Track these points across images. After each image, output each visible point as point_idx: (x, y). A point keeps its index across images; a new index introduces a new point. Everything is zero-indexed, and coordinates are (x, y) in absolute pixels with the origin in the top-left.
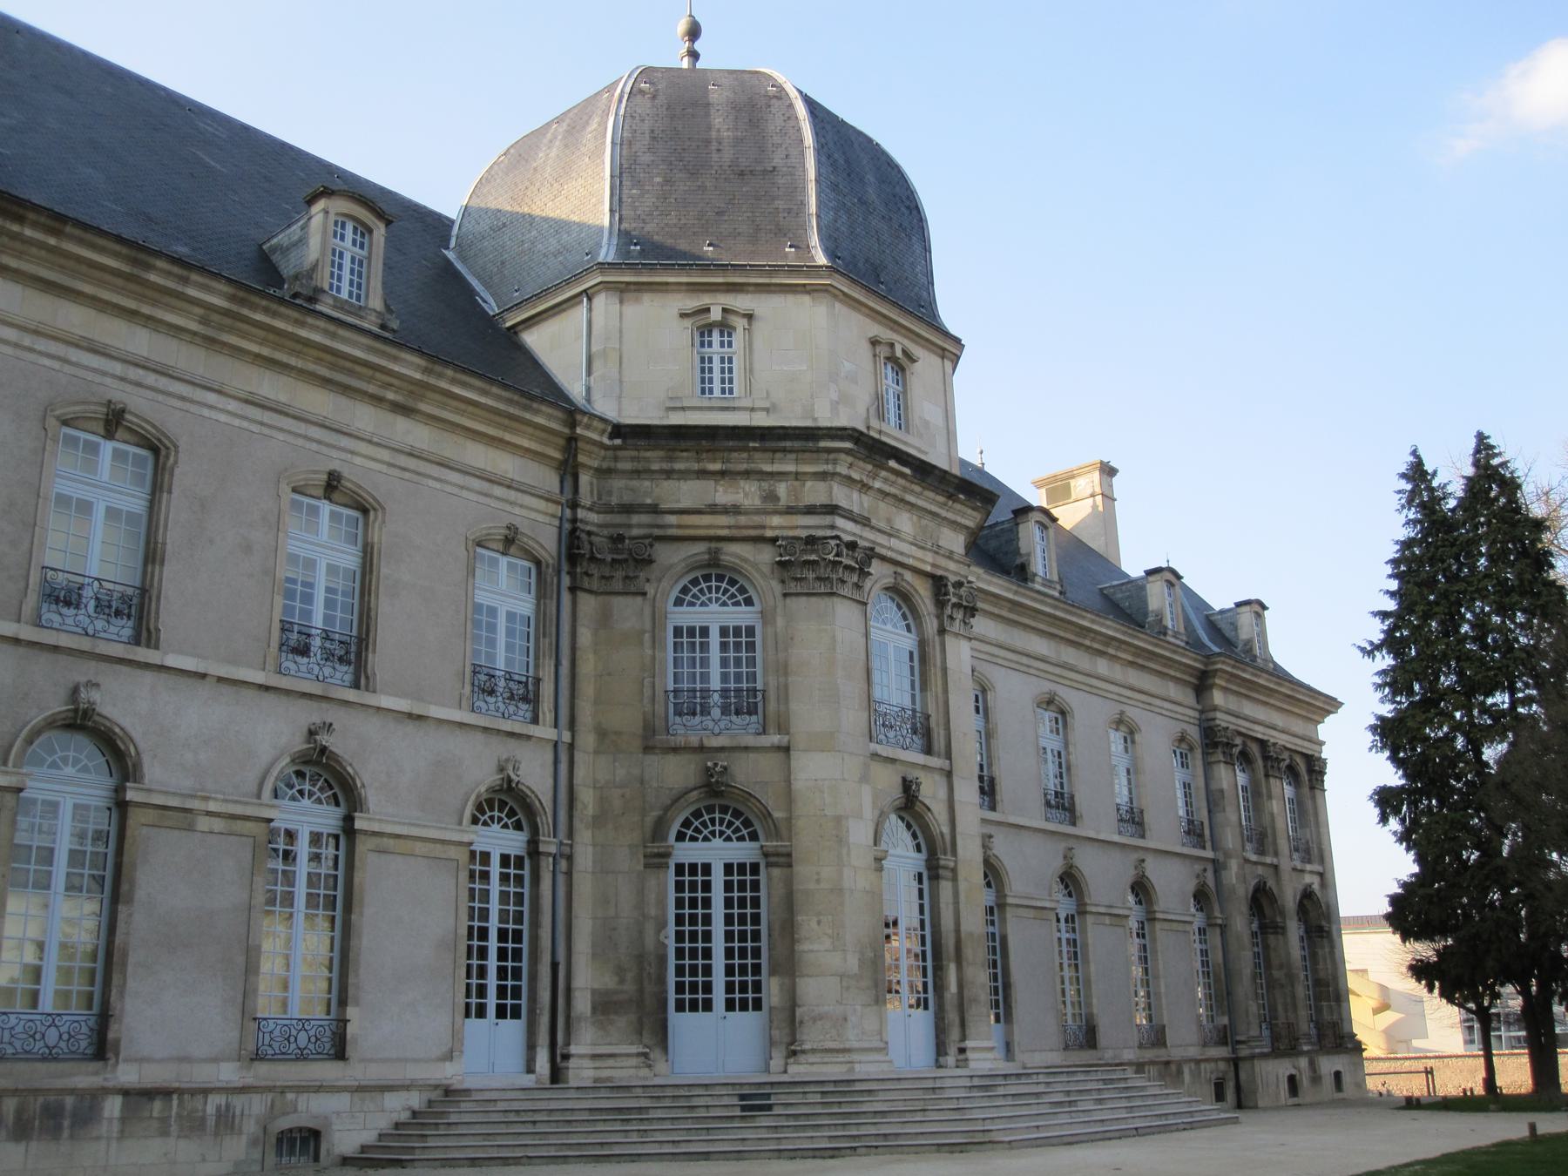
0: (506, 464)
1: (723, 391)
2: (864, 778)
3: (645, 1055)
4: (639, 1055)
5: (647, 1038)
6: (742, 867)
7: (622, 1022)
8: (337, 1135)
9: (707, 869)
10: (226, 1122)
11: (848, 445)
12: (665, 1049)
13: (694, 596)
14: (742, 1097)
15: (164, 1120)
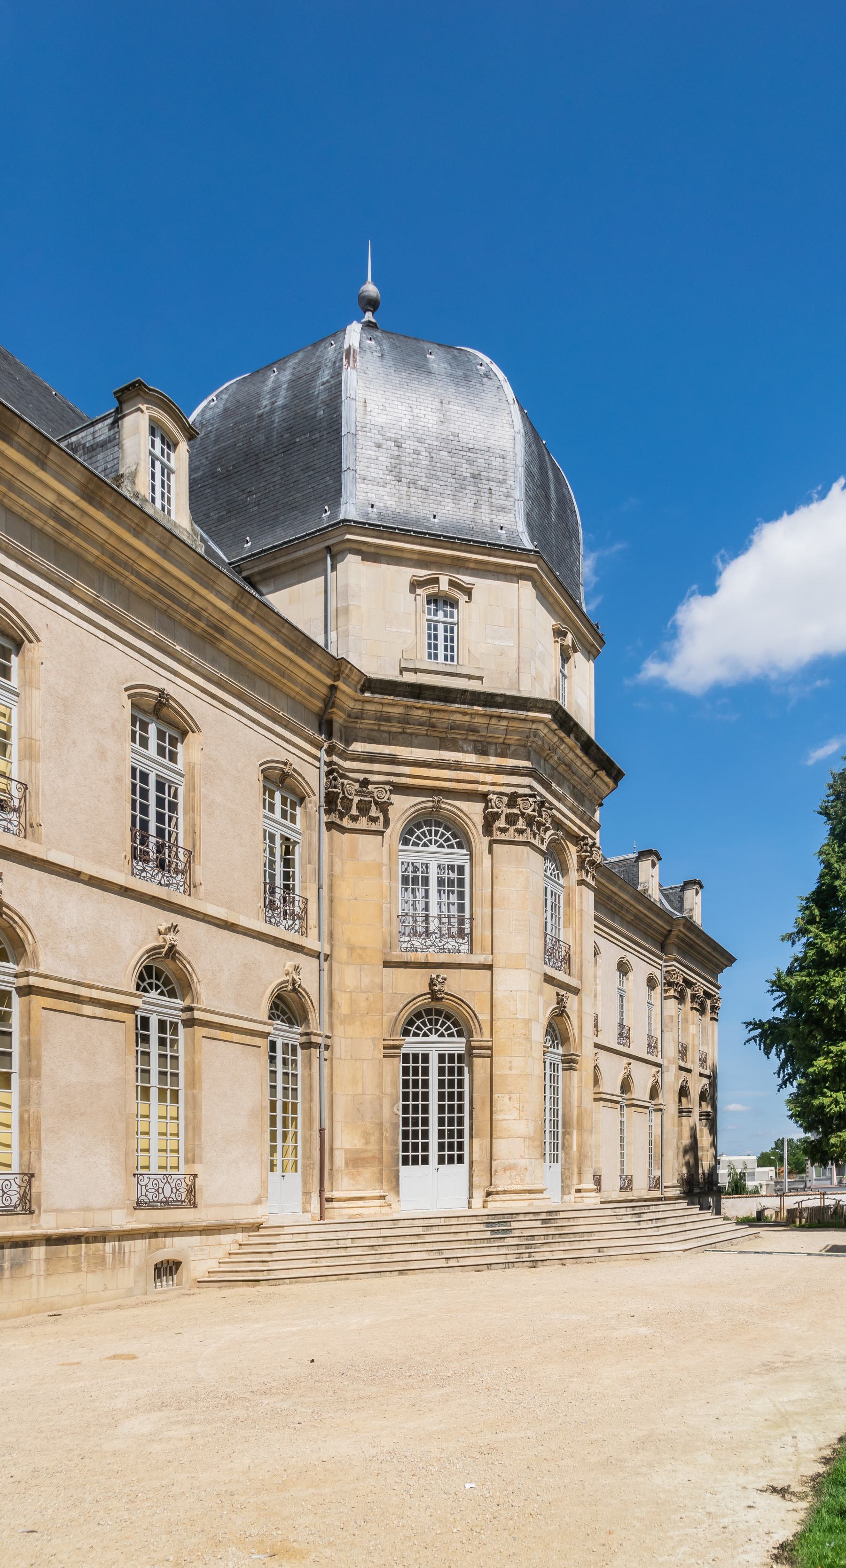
1: (446, 659)
3: (384, 1197)
5: (385, 1186)
8: (193, 1264)
9: (426, 1058)
12: (398, 1193)
13: (418, 838)
15: (77, 1259)
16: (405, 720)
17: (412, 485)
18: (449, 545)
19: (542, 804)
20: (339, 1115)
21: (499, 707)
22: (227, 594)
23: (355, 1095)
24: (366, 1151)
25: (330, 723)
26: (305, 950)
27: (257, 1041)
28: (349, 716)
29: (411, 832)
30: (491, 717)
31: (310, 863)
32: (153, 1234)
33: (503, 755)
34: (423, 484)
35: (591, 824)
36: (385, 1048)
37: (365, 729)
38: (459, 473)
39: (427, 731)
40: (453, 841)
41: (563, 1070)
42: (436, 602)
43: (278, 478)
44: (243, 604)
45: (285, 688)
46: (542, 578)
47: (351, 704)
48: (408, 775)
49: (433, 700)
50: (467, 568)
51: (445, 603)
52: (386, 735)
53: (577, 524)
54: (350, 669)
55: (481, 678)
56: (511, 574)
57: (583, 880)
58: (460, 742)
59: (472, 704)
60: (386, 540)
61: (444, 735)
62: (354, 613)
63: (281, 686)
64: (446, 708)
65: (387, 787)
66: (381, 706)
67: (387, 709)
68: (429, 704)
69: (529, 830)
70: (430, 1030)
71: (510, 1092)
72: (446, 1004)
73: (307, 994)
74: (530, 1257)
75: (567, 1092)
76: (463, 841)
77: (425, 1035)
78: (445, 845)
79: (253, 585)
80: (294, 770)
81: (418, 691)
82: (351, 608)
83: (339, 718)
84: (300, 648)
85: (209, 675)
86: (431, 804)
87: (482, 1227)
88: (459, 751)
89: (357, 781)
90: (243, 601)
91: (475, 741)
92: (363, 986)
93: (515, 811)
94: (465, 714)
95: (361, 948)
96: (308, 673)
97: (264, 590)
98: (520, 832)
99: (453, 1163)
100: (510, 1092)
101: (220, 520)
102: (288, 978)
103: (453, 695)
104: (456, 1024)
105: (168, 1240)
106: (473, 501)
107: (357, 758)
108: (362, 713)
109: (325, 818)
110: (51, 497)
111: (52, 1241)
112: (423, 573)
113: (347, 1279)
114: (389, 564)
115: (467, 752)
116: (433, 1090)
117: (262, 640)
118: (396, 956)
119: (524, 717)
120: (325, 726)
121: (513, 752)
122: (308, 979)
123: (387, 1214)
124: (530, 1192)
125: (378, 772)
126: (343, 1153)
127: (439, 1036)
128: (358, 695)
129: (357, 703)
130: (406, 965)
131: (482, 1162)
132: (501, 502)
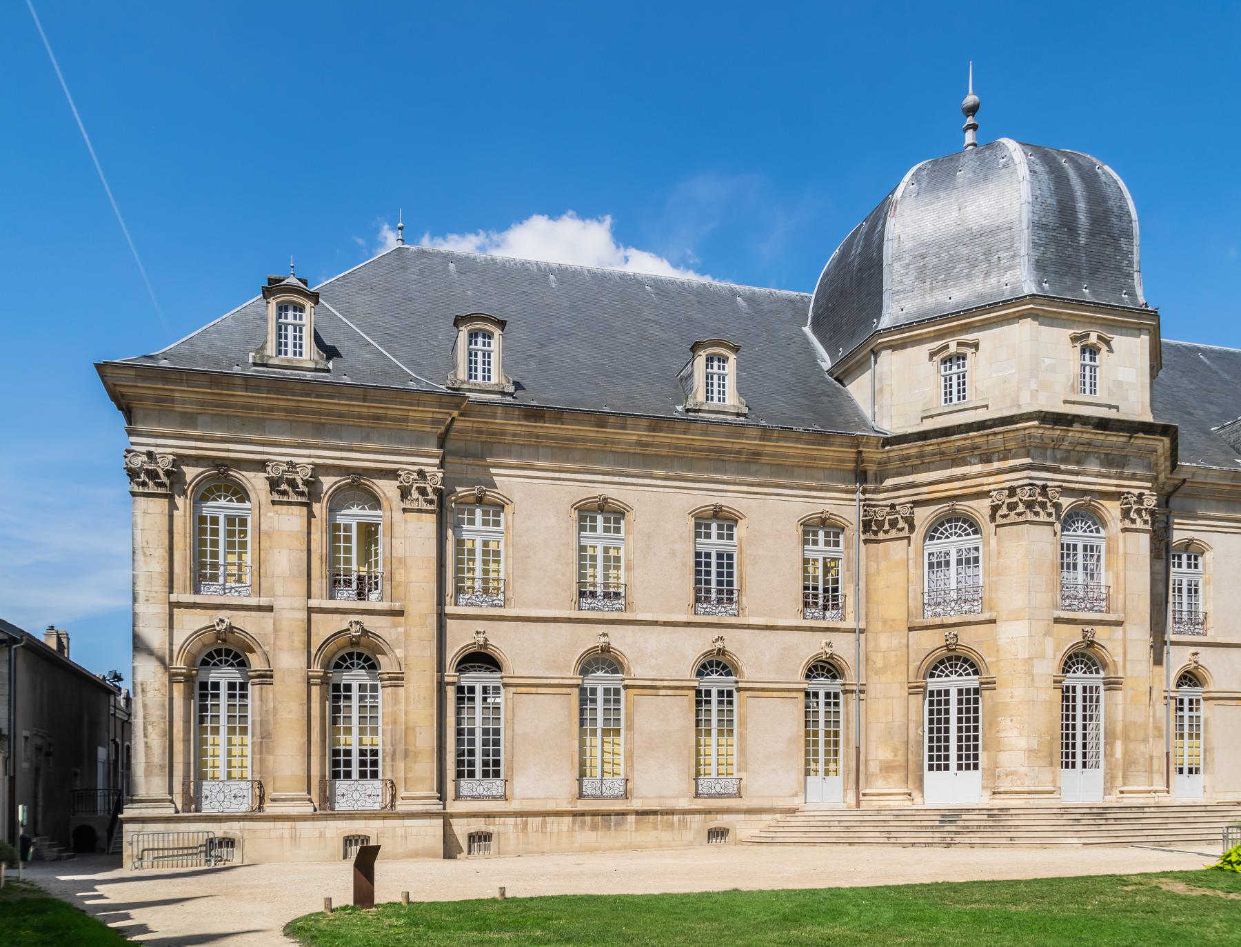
5: (911, 785)
6: (968, 691)
7: (897, 776)
9: (947, 693)
10: (683, 825)
11: (1036, 423)
12: (922, 791)
13: (942, 533)
14: (943, 815)
15: (655, 823)
16: (921, 455)
20: (873, 736)
25: (865, 472)
27: (794, 694)
29: (936, 530)
32: (708, 812)
33: (1005, 459)
48: (925, 493)
51: (958, 359)
55: (987, 406)
68: (934, 441)
72: (960, 652)
76: (974, 527)
77: (947, 676)
79: (840, 382)
81: (924, 436)
83: (872, 468)
87: (939, 818)
93: (1015, 499)
104: (972, 665)
105: (719, 816)
107: (887, 490)
109: (863, 537)
110: (634, 438)
111: (638, 813)
120: (861, 476)
122: (843, 648)
124: (1029, 793)
125: (904, 497)
130: (927, 628)
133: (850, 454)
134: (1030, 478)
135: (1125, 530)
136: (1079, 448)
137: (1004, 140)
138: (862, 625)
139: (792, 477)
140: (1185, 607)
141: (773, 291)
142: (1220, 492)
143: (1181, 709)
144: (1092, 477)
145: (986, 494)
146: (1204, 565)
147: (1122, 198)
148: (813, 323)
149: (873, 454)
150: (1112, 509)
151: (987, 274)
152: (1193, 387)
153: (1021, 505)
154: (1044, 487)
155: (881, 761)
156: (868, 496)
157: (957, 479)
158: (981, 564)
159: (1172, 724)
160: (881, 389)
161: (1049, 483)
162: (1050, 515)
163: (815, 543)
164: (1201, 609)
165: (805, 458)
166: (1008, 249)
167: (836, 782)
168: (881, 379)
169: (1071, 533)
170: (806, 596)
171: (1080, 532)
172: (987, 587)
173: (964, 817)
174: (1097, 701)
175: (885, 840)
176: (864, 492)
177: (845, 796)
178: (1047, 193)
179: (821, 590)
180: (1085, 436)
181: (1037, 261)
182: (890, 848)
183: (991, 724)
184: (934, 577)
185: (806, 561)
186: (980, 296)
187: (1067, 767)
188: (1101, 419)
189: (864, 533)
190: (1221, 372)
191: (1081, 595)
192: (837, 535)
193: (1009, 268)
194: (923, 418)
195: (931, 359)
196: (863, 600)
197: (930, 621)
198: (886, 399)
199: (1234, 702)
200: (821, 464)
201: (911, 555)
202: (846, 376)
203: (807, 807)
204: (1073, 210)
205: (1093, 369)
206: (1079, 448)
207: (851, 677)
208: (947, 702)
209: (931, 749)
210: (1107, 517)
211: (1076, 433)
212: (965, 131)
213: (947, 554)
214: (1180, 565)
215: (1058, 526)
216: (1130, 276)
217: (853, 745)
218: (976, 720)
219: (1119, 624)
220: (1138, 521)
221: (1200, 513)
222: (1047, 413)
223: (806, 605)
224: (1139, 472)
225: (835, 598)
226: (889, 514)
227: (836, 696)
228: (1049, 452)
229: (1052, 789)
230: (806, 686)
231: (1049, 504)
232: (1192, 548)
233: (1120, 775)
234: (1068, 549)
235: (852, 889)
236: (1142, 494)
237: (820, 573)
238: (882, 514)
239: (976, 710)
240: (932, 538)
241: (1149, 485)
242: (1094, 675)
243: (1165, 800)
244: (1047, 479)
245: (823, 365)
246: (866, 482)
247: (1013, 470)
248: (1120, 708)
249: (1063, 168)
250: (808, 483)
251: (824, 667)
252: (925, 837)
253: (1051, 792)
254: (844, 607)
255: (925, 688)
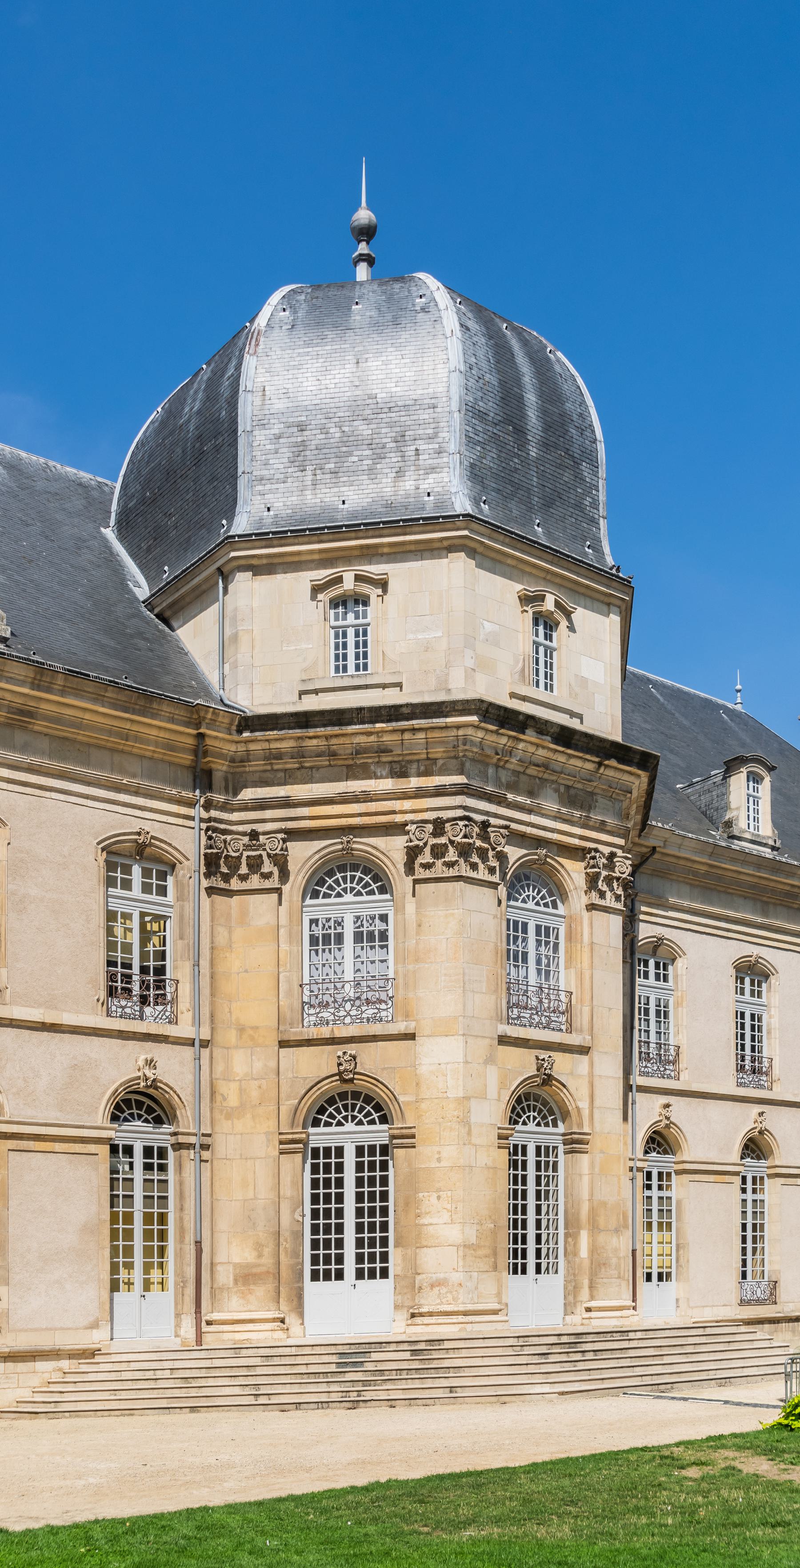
0: (185, 756)
1: (357, 668)
2: (490, 1060)
4: (274, 1320)
5: (284, 1306)
7: (261, 1291)
9: (340, 1152)
11: (474, 719)
12: (301, 1315)
13: (330, 888)
16: (299, 754)
17: (318, 472)
18: (353, 535)
19: (485, 825)
20: (222, 1225)
21: (408, 719)
22: (22, 678)
23: (245, 1200)
24: (259, 1265)
25: (209, 773)
26: (170, 1039)
27: (92, 1148)
28: (232, 760)
29: (321, 882)
30: (403, 731)
31: (181, 938)
33: (427, 773)
34: (332, 466)
35: (608, 828)
36: (281, 1143)
37: (256, 772)
38: (377, 441)
39: (329, 760)
40: (374, 886)
41: (566, 1153)
42: (344, 604)
43: (191, 494)
44: (45, 682)
45: (135, 750)
46: (482, 543)
47: (233, 748)
49: (325, 726)
50: (382, 555)
51: (357, 602)
52: (281, 774)
53: (595, 441)
54: (214, 713)
55: (399, 685)
56: (438, 549)
57: (593, 904)
58: (372, 767)
59: (373, 722)
60: (280, 548)
61: (351, 762)
62: (244, 638)
63: (130, 749)
64: (344, 732)
65: (281, 836)
66: (267, 743)
67: (274, 745)
68: (320, 731)
69: (462, 861)
70: (345, 1118)
71: (439, 1190)
72: (360, 1084)
73: (171, 1088)
74: (359, 1396)
75: (569, 1182)
77: (339, 1124)
78: (363, 891)
79: (166, 622)
80: (153, 837)
81: (304, 720)
82: (240, 633)
83: (220, 767)
84: (137, 707)
85: (15, 764)
86: (340, 847)
87: (334, 1359)
88: (371, 778)
89: (244, 834)
90: (44, 679)
91: (391, 762)
92: (254, 1072)
93: (443, 840)
94: (369, 734)
95: (252, 1028)
96: (160, 728)
97: (175, 624)
98: (450, 865)
99: (330, 1279)
100: (439, 1190)
101: (149, 550)
102: (140, 1074)
103: (347, 716)
104: (378, 1108)
106: (394, 470)
107: (245, 808)
108: (248, 755)
109: (205, 883)
112: (322, 574)
113: (132, 1415)
114: (285, 573)
115: (381, 777)
116: (350, 1190)
117: (85, 710)
118: (295, 1033)
119: (444, 725)
120: (203, 779)
121: (440, 768)
122: (174, 1070)
123: (280, 1340)
124: (465, 1313)
125: (271, 821)
126: (231, 1268)
127: (356, 1124)
128: (236, 737)
129: (239, 745)
131: (406, 1276)
132: (430, 462)
133: (186, 736)
134: (465, 808)
135: (591, 907)
136: (532, 771)
137: (421, 275)
138: (205, 1034)
139: (87, 764)
140: (653, 1038)
141: (51, 463)
142: (696, 873)
143: (649, 1187)
144: (548, 821)
145: (399, 829)
146: (676, 977)
147: (583, 403)
148: (119, 522)
149: (222, 742)
150: (574, 873)
151: (400, 473)
152: (648, 727)
153: (451, 849)
154: (485, 825)
155: (235, 1265)
156: (214, 813)
157: (355, 799)
158: (391, 942)
159: (640, 1208)
160: (235, 638)
161: (493, 821)
162: (492, 870)
163: (127, 885)
164: (671, 1042)
165: (110, 733)
166: (431, 438)
167: (163, 1301)
168: (234, 619)
169: (519, 904)
170: (112, 977)
171: (531, 905)
172: (401, 981)
173: (375, 1356)
174: (555, 1169)
175: (251, 1400)
176: (208, 806)
177: (178, 1326)
178: (484, 365)
179: (136, 969)
180: (541, 752)
181: (472, 466)
182: (257, 1414)
183: (407, 1204)
184: (318, 960)
185: (111, 916)
186: (389, 506)
187: (515, 1272)
188: (564, 728)
189: (208, 875)
190: (677, 715)
191: (534, 1002)
192: (162, 876)
193: (433, 469)
194: (302, 693)
195: (313, 598)
196: (206, 991)
197: (313, 1033)
198: (242, 654)
199: (712, 1178)
200: (138, 748)
201: (283, 921)
202: (175, 613)
203: (115, 1347)
204: (520, 400)
205: (549, 652)
206: (532, 771)
207: (186, 1121)
208: (340, 1168)
209: (315, 1245)
210: (569, 885)
211: (529, 745)
212: (356, 263)
213: (339, 923)
214: (646, 976)
215: (502, 891)
216: (594, 522)
217: (190, 1238)
218: (384, 1196)
219: (584, 1050)
220: (609, 894)
221: (672, 900)
222: (491, 704)
223: (111, 992)
224: (610, 821)
225: (160, 985)
226: (247, 847)
227: (162, 1153)
228: (491, 771)
229: (496, 1306)
230: (111, 1134)
231: (491, 853)
232: (661, 951)
233: (586, 1283)
234: (516, 930)
235: (232, 1509)
236: (613, 855)
237: (135, 938)
238: (237, 846)
239: (384, 1181)
240: (315, 895)
241: (621, 842)
242: (551, 1129)
243: (631, 1321)
244: (487, 813)
245: (136, 590)
246: (210, 788)
247: (440, 792)
248: (586, 1180)
249: (504, 336)
250: (116, 777)
251: (142, 1103)
252: (316, 1391)
253: (495, 1312)
254: (174, 1001)
255: (305, 1143)
